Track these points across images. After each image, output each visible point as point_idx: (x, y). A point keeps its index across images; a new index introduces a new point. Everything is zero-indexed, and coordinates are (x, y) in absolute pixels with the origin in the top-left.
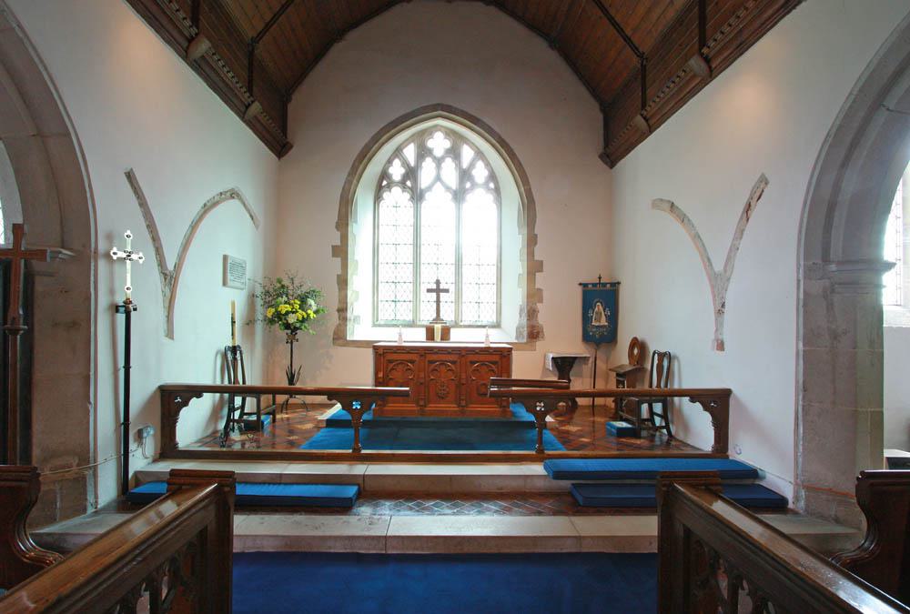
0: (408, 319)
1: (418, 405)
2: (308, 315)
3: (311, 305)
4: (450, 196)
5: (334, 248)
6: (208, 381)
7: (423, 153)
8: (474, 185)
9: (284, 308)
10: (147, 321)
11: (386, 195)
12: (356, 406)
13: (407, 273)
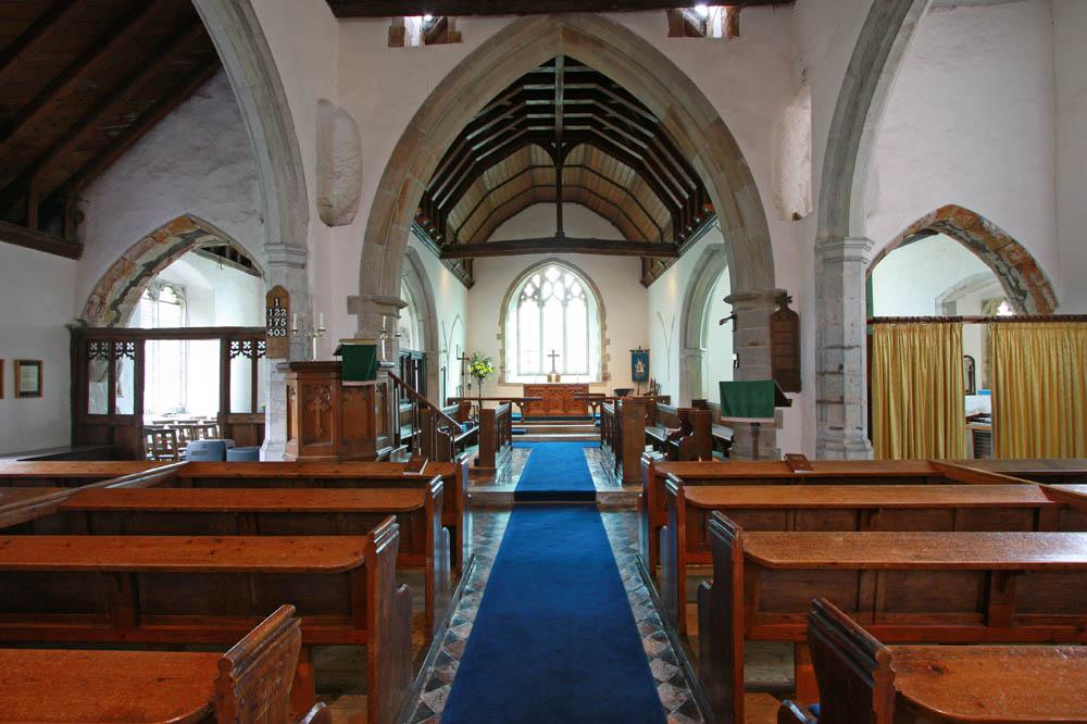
11: (523, 304)
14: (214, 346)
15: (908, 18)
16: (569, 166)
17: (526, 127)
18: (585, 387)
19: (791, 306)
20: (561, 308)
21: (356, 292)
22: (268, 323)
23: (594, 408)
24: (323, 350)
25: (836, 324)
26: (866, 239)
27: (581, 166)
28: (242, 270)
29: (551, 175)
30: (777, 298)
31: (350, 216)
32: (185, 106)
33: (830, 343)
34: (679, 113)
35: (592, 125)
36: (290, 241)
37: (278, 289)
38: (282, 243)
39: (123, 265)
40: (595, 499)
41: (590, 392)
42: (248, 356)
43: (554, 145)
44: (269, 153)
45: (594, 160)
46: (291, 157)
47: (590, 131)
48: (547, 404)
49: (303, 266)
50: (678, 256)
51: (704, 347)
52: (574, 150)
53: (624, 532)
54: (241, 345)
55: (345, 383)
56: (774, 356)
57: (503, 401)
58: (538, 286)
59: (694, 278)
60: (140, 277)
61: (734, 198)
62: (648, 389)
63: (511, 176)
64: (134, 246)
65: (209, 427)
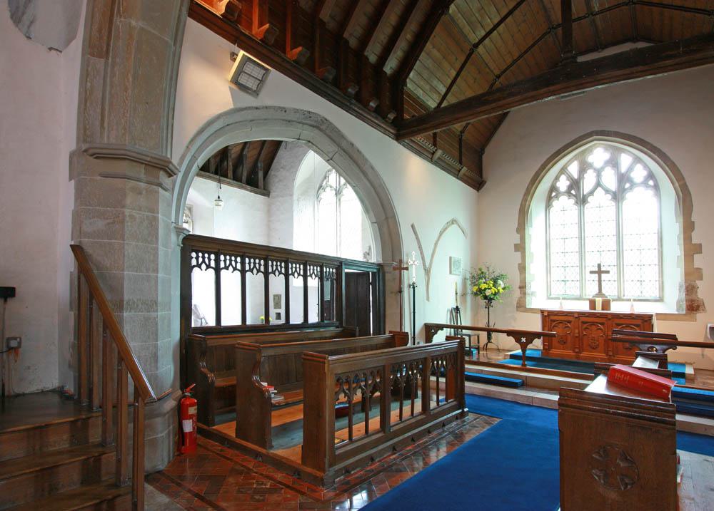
0: (575, 294)
1: (574, 352)
2: (499, 291)
3: (500, 284)
4: (609, 197)
5: (516, 246)
6: (443, 322)
7: (583, 169)
8: (633, 185)
9: (483, 286)
10: (420, 292)
11: (555, 203)
12: (524, 340)
13: (574, 259)
18: (646, 320)
28: (247, 190)
41: (656, 331)
58: (576, 176)
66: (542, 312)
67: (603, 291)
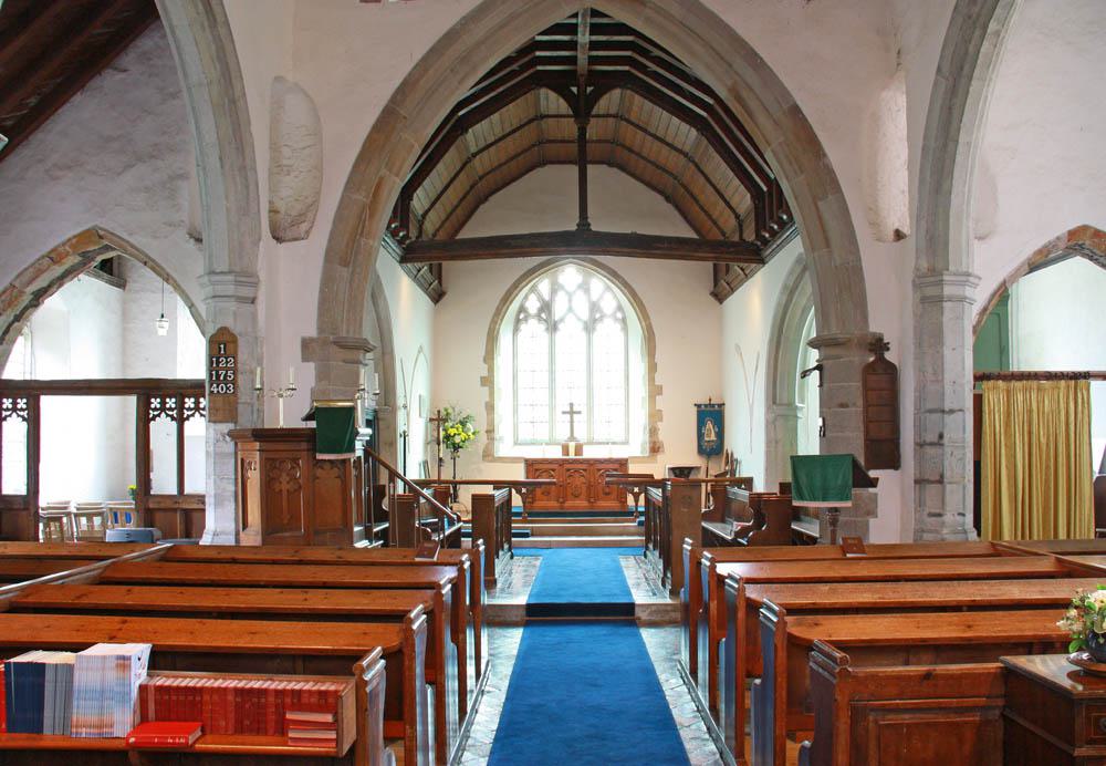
11: (523, 326)
13: (543, 396)
14: (132, 401)
15: (992, 26)
16: (598, 116)
17: (533, 51)
18: (623, 463)
19: (888, 356)
20: (584, 335)
21: (312, 332)
22: (211, 375)
23: (636, 497)
24: (288, 413)
25: (937, 381)
26: (969, 275)
27: (615, 116)
28: (103, 279)
29: (569, 128)
30: (871, 344)
31: (304, 227)
32: (95, 83)
33: (929, 406)
34: (745, 94)
35: (630, 66)
36: (237, 269)
37: (223, 331)
38: (230, 272)
39: (11, 295)
40: (633, 614)
41: (630, 472)
42: (173, 418)
43: (574, 89)
44: (221, 159)
45: (635, 108)
46: (244, 160)
47: (628, 71)
48: (563, 491)
49: (253, 301)
50: (762, 262)
51: (803, 402)
52: (606, 96)
53: (668, 645)
54: (163, 403)
55: (320, 456)
56: (868, 422)
57: (498, 485)
58: (547, 298)
59: (784, 298)
60: (26, 309)
61: (817, 208)
62: (722, 468)
63: (508, 130)
64: (26, 269)
65: (83, 515)
66: (526, 461)
67: (575, 435)
